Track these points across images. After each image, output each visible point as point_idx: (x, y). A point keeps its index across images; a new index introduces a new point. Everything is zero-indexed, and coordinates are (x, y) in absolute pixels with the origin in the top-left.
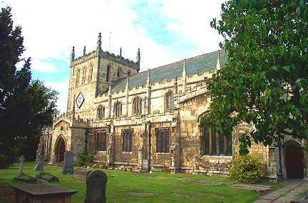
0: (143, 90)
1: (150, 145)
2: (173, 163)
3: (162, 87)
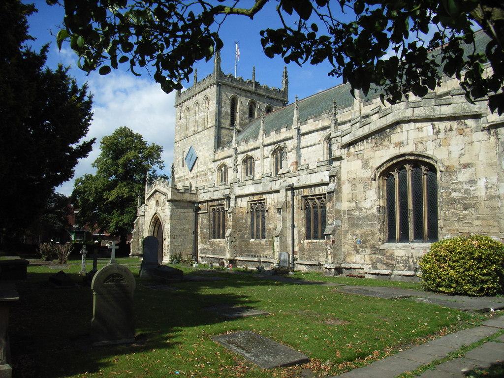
0: (288, 135)
1: (293, 226)
2: (330, 257)
3: (320, 126)
